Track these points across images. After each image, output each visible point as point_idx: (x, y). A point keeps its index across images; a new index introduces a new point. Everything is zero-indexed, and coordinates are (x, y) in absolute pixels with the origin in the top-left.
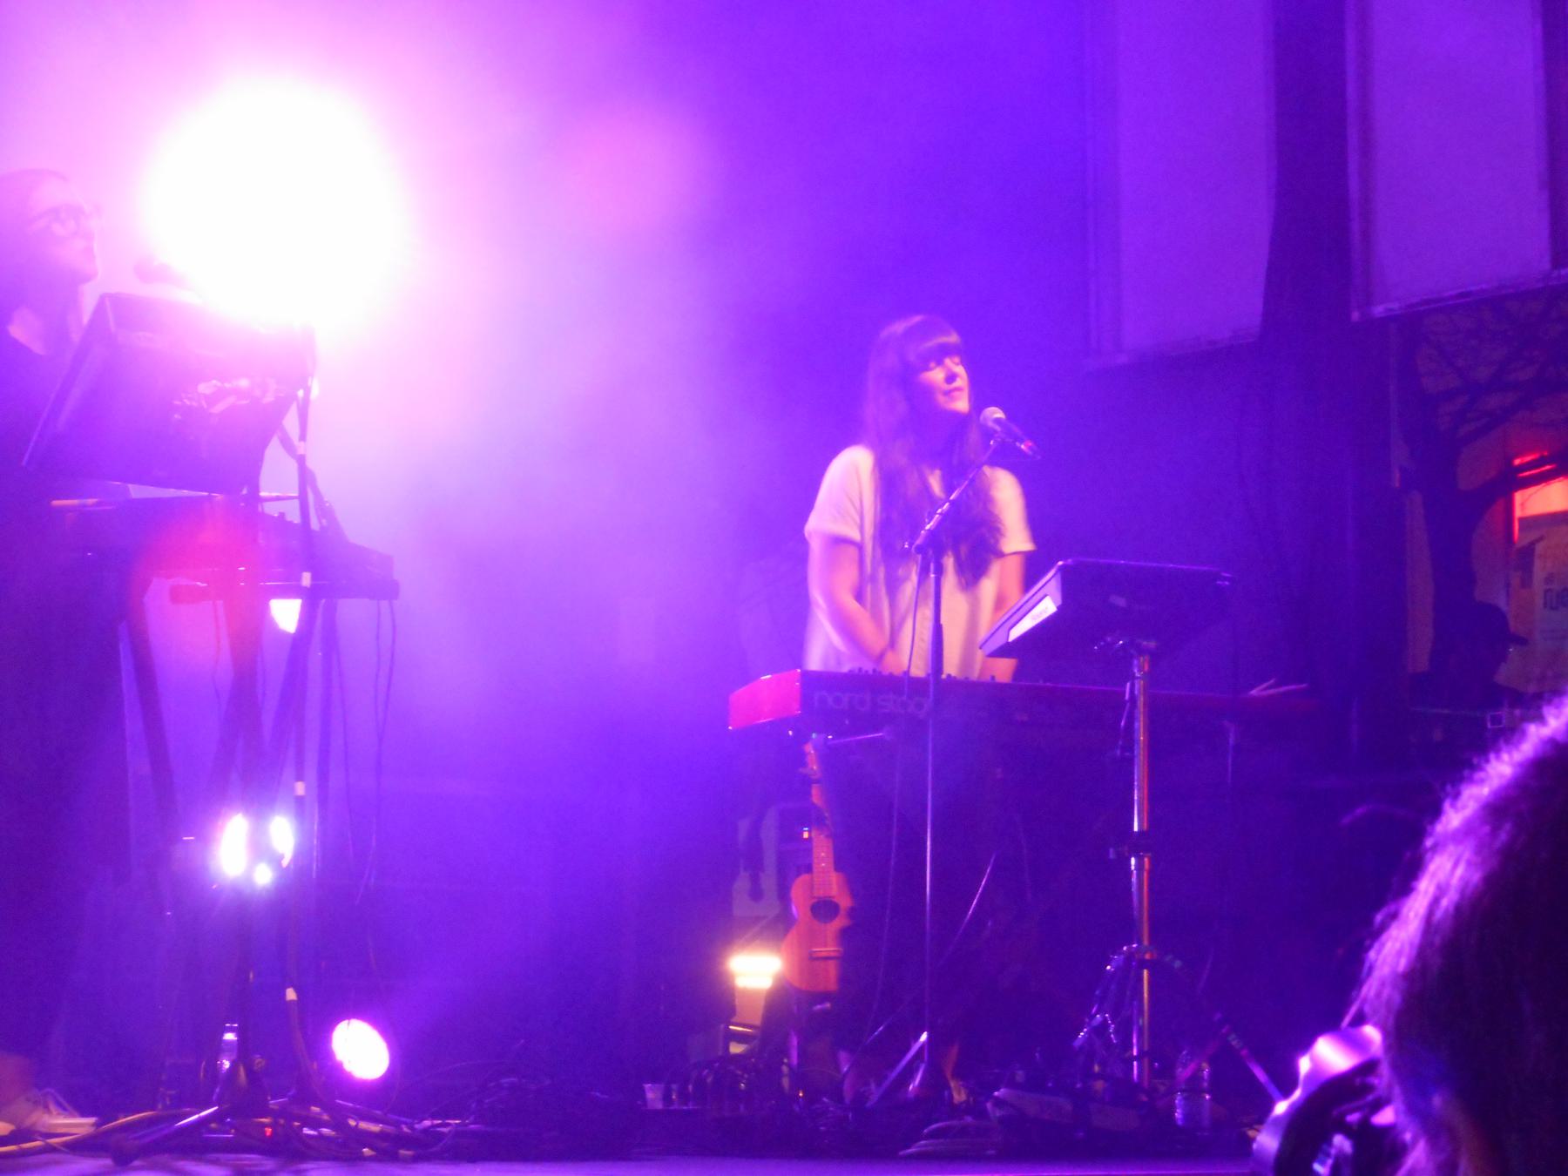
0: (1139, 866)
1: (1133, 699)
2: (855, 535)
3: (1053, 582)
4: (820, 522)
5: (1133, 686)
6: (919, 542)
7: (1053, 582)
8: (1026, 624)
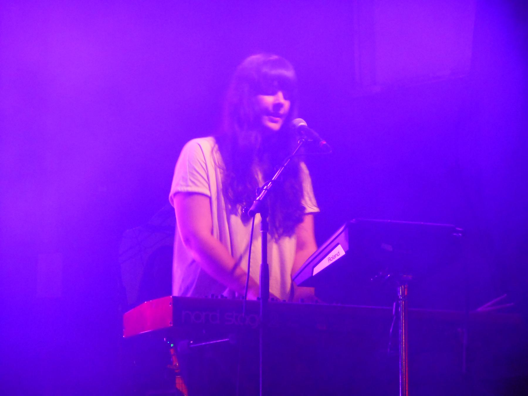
0: (405, 288)
1: (398, 313)
2: (207, 192)
3: (343, 234)
4: (178, 185)
5: (398, 306)
6: (252, 208)
7: (343, 234)
8: (325, 263)
